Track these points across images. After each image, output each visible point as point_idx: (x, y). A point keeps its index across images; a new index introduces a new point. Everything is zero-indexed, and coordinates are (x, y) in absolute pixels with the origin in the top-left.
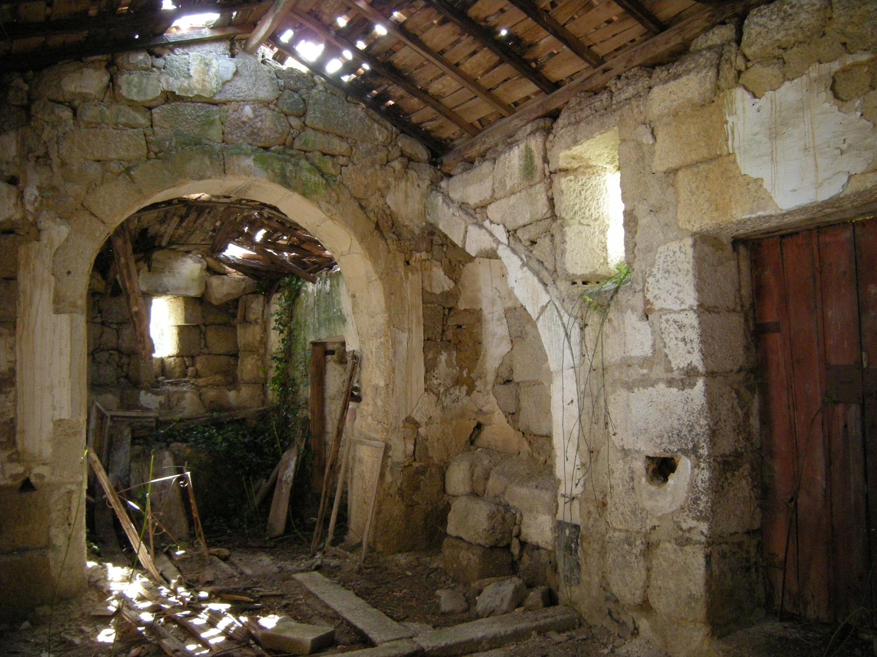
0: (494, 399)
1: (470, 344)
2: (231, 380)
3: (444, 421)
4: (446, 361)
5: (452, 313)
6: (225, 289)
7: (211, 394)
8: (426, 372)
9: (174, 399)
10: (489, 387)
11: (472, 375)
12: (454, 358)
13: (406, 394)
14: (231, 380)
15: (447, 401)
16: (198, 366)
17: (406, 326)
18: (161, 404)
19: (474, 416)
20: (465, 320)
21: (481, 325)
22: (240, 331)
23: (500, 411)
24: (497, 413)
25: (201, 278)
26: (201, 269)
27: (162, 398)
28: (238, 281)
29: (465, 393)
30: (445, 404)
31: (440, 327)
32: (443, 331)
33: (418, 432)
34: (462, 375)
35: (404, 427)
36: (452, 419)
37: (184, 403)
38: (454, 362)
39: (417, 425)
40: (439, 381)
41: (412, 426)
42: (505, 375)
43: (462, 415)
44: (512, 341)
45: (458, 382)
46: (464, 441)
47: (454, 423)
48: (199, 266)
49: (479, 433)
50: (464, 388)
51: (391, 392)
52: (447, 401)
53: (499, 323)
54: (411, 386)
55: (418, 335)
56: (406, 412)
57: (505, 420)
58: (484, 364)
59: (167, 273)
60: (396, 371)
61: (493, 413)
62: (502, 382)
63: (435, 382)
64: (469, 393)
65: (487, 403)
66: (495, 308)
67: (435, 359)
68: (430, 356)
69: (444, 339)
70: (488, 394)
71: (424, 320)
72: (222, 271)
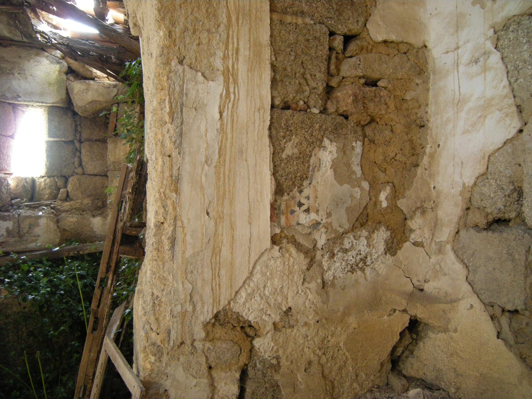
0: (458, 267)
1: (399, 128)
2: (100, 204)
3: (324, 319)
4: (335, 166)
5: (353, 47)
6: (90, 96)
7: (71, 220)
8: (279, 191)
9: (25, 225)
10: (445, 234)
11: (402, 204)
12: (356, 160)
13: (216, 252)
14: (100, 204)
15: (335, 268)
16: (70, 187)
17: (218, 63)
18: (8, 231)
19: (403, 304)
20: (384, 68)
21: (426, 81)
22: (110, 146)
23: (474, 300)
24: (463, 305)
25: (59, 82)
26: (60, 71)
27: (9, 224)
28: (109, 87)
29: (382, 247)
30: (329, 276)
31: (320, 76)
32: (329, 90)
33: (252, 349)
34: (377, 203)
35: (209, 337)
36: (346, 313)
37: (37, 231)
38: (357, 170)
39: (248, 331)
40: (313, 216)
41: (238, 334)
42: (495, 203)
43: (374, 302)
44: (520, 109)
45: (364, 219)
46: (376, 364)
47: (352, 321)
48: (58, 67)
49: (415, 341)
50: (381, 236)
51: (167, 245)
52: (335, 268)
53: (475, 68)
54: (232, 227)
55: (255, 94)
56: (216, 300)
57: (489, 329)
58: (432, 176)
59: (16, 75)
60: (186, 187)
61: (454, 301)
62: (482, 222)
63: (304, 219)
64: (392, 248)
65: (438, 272)
66: (464, 35)
67: (304, 157)
68: (290, 149)
69: (331, 108)
70: (440, 251)
71: (276, 52)
72: (88, 75)
